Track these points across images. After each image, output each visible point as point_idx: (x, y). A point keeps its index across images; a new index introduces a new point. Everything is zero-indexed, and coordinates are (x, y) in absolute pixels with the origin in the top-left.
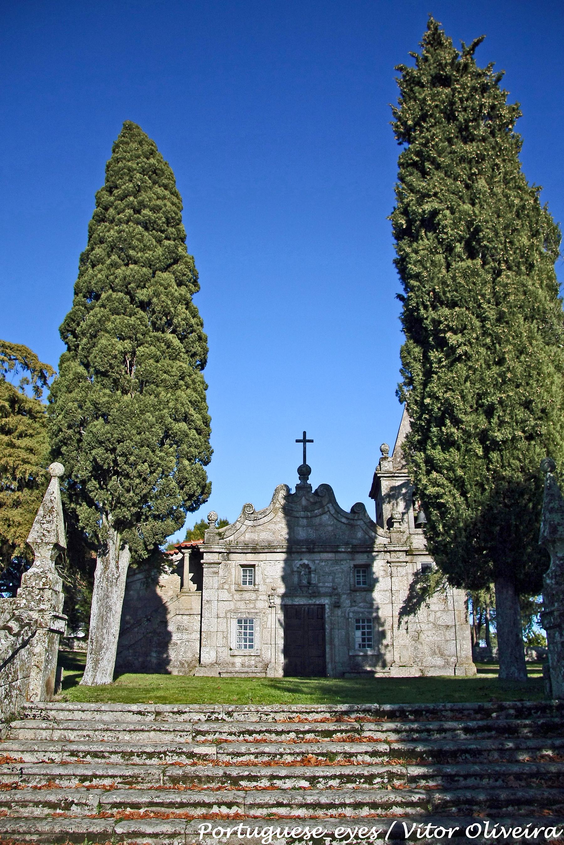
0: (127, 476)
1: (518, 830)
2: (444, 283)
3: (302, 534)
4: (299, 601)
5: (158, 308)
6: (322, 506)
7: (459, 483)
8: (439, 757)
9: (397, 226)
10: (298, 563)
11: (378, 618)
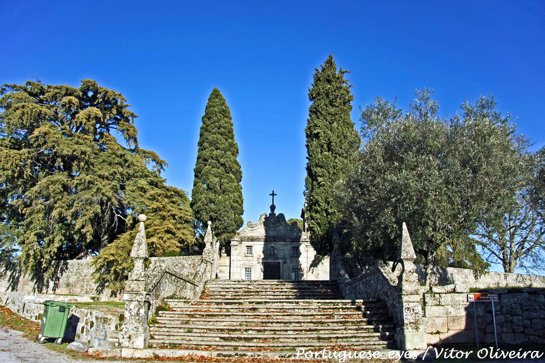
0: (220, 220)
1: (513, 353)
2: (319, 159)
3: (271, 234)
4: (270, 261)
5: (228, 166)
6: (280, 222)
7: (319, 224)
8: (300, 289)
9: (307, 134)
10: (269, 246)
11: (301, 268)
